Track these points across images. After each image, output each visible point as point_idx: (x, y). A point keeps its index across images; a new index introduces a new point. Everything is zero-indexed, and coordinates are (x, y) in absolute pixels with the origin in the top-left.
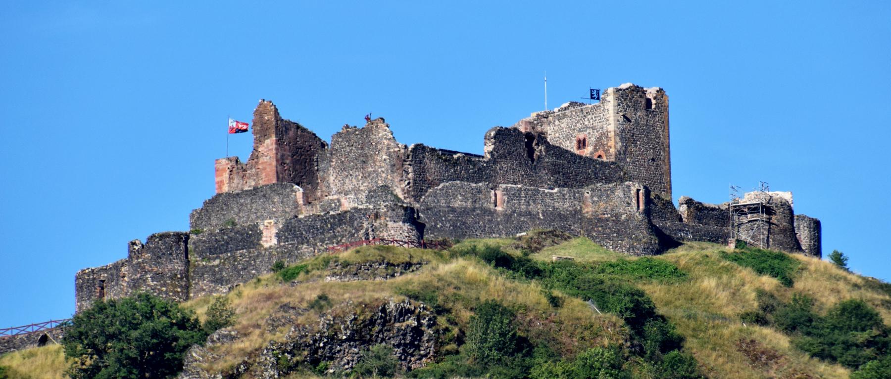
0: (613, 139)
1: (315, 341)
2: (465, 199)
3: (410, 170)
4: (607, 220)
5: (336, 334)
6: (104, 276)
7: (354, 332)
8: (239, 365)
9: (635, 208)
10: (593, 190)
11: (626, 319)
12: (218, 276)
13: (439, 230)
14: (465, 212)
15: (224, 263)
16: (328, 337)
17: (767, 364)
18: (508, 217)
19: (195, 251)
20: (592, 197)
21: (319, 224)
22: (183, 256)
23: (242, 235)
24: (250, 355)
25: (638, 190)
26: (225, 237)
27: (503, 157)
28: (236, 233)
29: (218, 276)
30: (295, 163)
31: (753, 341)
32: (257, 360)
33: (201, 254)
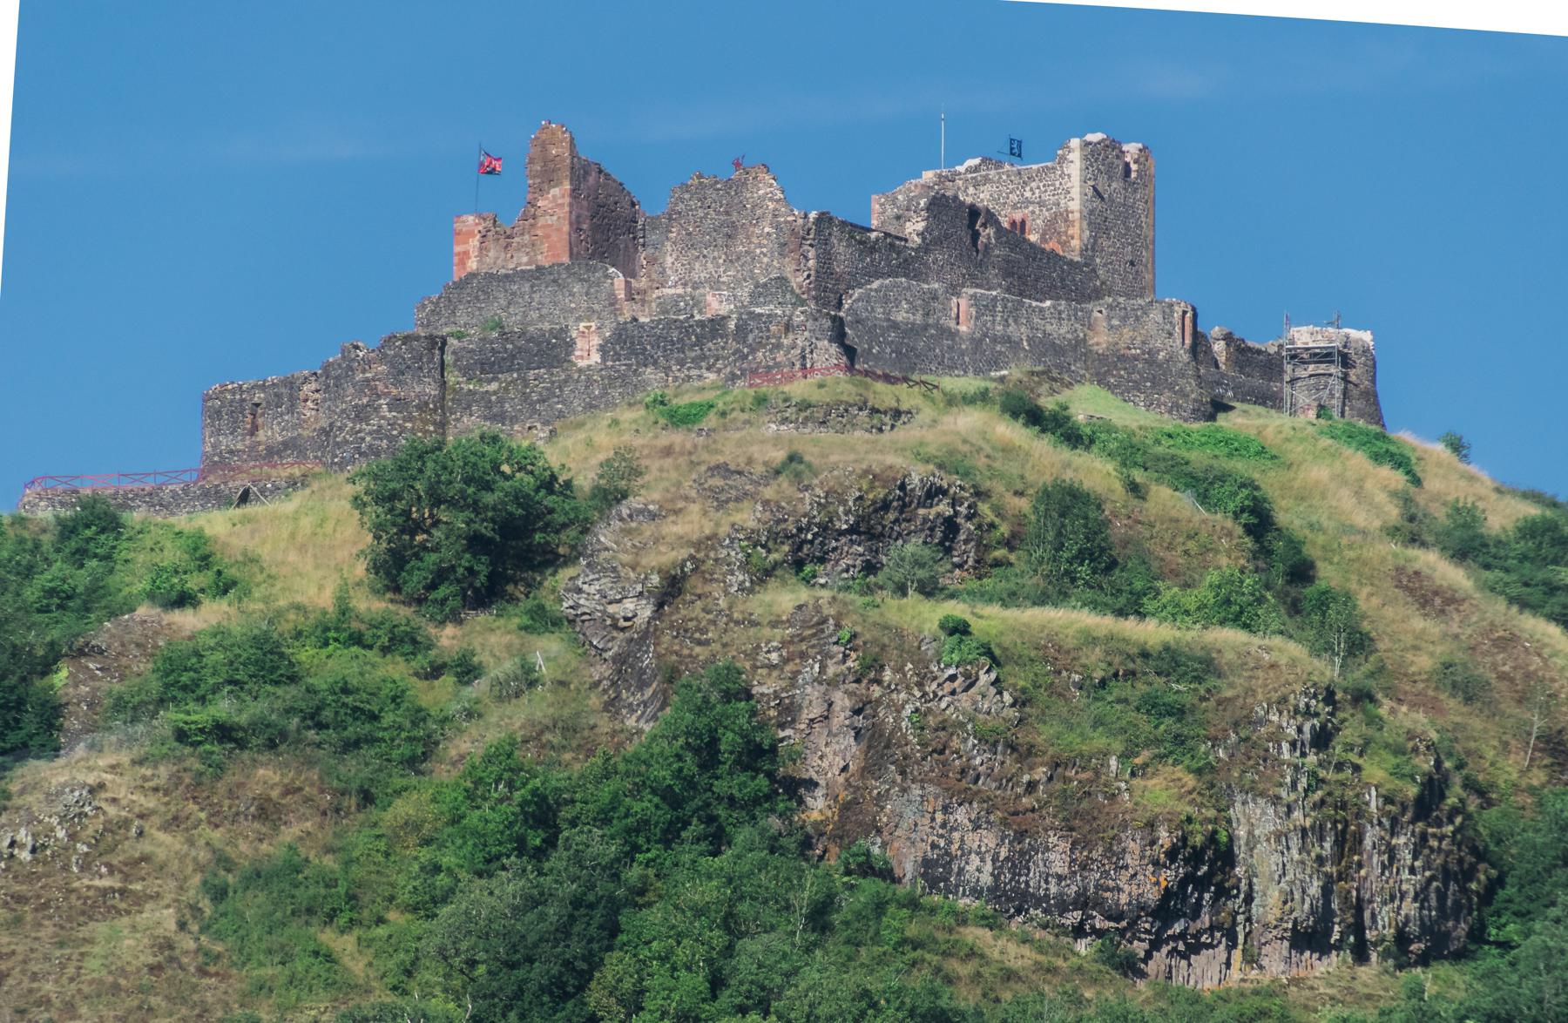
0: (1077, 224)
1: (800, 530)
2: (913, 309)
3: (810, 255)
4: (1136, 358)
5: (831, 521)
6: (259, 396)
7: (861, 519)
8: (684, 561)
9: (1179, 342)
10: (1110, 307)
11: (1245, 525)
12: (495, 410)
13: (877, 358)
14: (913, 331)
15: (506, 389)
16: (819, 525)
17: (1443, 611)
18: (977, 343)
19: (455, 365)
20: (1109, 318)
21: (675, 335)
22: (438, 376)
23: (539, 344)
24: (698, 545)
25: (1185, 313)
26: (510, 346)
27: (937, 242)
28: (528, 341)
29: (495, 410)
30: (595, 228)
31: (1417, 573)
32: (712, 554)
33: (466, 372)
